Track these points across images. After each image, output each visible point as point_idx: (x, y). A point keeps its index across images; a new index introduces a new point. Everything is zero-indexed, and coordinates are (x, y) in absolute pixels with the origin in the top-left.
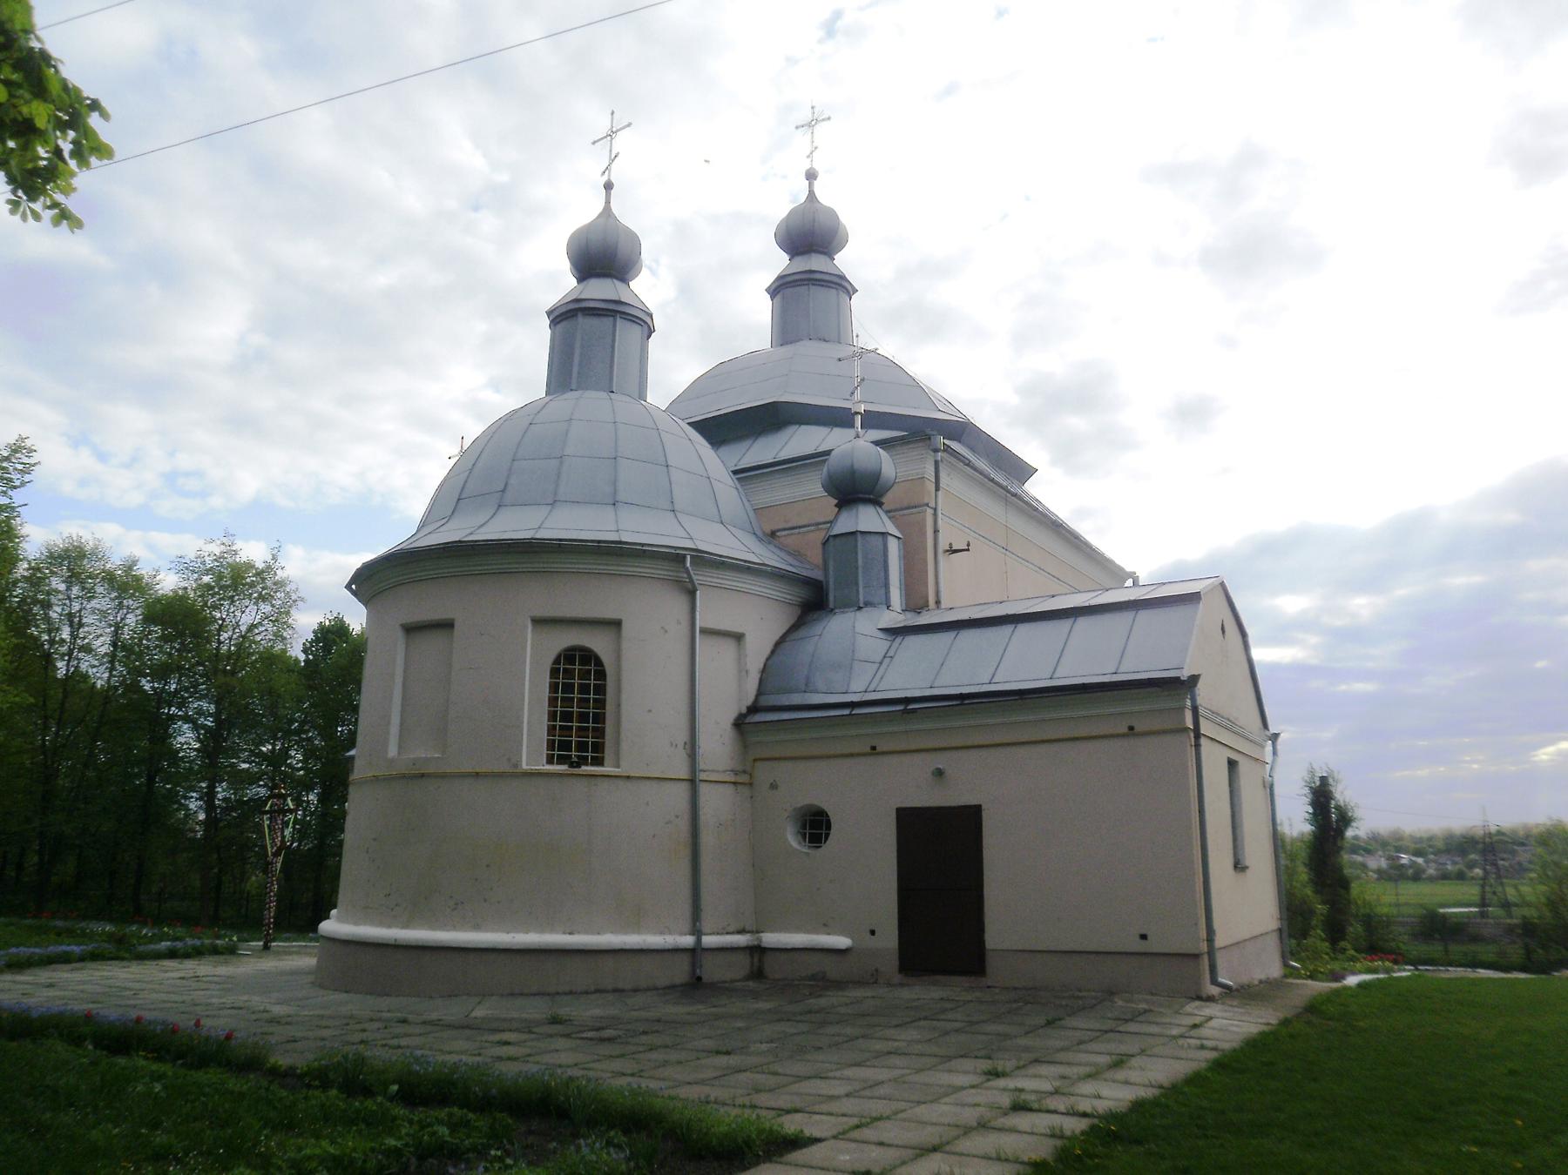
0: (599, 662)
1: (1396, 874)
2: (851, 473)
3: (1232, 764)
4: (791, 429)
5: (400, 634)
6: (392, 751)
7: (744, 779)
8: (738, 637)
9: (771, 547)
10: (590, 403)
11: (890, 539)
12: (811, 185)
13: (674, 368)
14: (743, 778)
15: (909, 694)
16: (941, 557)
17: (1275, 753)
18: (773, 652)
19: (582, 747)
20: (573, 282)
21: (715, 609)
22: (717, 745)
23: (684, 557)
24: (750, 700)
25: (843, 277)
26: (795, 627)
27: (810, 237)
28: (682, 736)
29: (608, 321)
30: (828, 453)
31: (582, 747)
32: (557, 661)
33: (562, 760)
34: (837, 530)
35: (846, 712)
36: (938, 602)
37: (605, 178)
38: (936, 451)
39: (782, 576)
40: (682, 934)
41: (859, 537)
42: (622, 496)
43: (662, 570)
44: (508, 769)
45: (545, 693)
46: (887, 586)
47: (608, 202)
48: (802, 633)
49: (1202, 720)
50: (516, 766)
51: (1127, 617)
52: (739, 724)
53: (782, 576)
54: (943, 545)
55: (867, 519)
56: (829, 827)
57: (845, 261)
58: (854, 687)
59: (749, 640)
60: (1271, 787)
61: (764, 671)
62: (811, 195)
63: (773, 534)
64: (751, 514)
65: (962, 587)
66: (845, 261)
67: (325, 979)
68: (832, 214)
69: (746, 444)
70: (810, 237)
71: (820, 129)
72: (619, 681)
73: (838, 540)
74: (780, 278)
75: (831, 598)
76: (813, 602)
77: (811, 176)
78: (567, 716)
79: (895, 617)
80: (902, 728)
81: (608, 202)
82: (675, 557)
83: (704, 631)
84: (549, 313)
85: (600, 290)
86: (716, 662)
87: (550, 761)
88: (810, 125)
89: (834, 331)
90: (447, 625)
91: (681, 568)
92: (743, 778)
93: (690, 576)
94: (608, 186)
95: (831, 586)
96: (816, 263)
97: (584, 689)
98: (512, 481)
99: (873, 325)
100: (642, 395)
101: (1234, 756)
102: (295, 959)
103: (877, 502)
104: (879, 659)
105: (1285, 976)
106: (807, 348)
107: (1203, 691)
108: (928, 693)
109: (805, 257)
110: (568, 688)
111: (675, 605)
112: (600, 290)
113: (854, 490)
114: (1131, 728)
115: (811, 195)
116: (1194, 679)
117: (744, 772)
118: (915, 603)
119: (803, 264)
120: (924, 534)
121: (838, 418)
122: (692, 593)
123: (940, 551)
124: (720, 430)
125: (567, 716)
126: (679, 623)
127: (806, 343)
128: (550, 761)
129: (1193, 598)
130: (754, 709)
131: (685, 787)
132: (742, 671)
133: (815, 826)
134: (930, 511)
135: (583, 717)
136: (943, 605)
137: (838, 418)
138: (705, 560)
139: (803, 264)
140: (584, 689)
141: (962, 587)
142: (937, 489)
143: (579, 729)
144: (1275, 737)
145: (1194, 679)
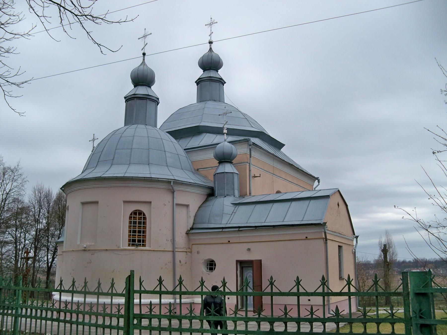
0: (144, 215)
2: (225, 150)
3: (340, 247)
4: (204, 134)
5: (80, 206)
6: (78, 243)
7: (189, 251)
8: (187, 206)
9: (197, 176)
10: (140, 130)
14: (188, 250)
15: (240, 225)
17: (357, 242)
18: (198, 210)
19: (139, 241)
20: (132, 86)
21: (180, 198)
22: (181, 240)
23: (171, 182)
24: (190, 226)
25: (221, 79)
27: (210, 64)
28: (170, 238)
29: (145, 101)
31: (139, 241)
32: (131, 214)
33: (133, 245)
34: (219, 171)
35: (221, 230)
36: (250, 193)
37: (143, 52)
39: (201, 186)
40: (170, 299)
42: (151, 162)
43: (165, 186)
44: (116, 248)
45: (127, 224)
46: (233, 189)
47: (144, 60)
48: (207, 204)
49: (327, 234)
50: (119, 247)
51: (307, 202)
52: (187, 233)
53: (201, 186)
54: (252, 175)
55: (228, 168)
56: (215, 265)
57: (222, 73)
58: (223, 223)
59: (191, 208)
60: (355, 252)
61: (195, 216)
63: (198, 170)
64: (190, 163)
65: (259, 189)
66: (222, 73)
69: (189, 139)
70: (210, 64)
71: (214, 26)
72: (150, 221)
73: (218, 175)
76: (211, 194)
80: (238, 235)
81: (144, 60)
82: (168, 182)
83: (177, 204)
85: (142, 91)
86: (181, 213)
87: (129, 245)
88: (211, 24)
89: (219, 98)
90: (97, 203)
91: (171, 185)
92: (188, 250)
93: (173, 188)
94: (144, 54)
95: (216, 188)
96: (212, 74)
97: (140, 223)
98: (116, 156)
101: (341, 245)
103: (231, 162)
104: (231, 213)
105: (436, 325)
106: (210, 104)
107: (329, 226)
109: (208, 71)
110: (135, 223)
111: (167, 197)
112: (142, 91)
113: (224, 158)
116: (325, 224)
117: (189, 248)
118: (242, 195)
120: (246, 170)
121: (218, 131)
122: (173, 192)
124: (177, 134)
125: (130, 235)
126: (169, 202)
127: (209, 102)
128: (129, 245)
129: (327, 197)
130: (192, 229)
131: (171, 253)
132: (188, 217)
133: (211, 265)
134: (248, 164)
135: (139, 232)
136: (252, 194)
137: (218, 131)
138: (177, 182)
140: (140, 223)
141: (259, 189)
142: (250, 157)
143: (138, 235)
144: (357, 237)
145: (325, 224)
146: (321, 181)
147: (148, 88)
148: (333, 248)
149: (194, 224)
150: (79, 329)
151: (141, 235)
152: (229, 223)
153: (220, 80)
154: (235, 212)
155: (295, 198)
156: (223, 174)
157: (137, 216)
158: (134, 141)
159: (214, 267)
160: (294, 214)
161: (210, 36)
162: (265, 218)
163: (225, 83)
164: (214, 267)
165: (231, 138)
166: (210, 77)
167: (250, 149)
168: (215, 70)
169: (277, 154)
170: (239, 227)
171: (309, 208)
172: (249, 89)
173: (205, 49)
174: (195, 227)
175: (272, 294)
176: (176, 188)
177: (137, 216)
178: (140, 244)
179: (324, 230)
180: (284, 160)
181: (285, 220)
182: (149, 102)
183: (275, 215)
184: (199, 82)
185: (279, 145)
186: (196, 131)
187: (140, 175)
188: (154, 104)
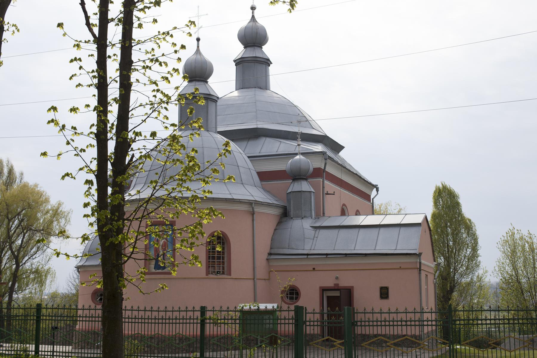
1: (447, 343)
12: (253, 13)
16: (325, 195)
36: (324, 213)
39: (277, 207)
46: (311, 210)
47: (198, 47)
66: (268, 50)
73: (294, 193)
75: (292, 214)
81: (198, 47)
82: (250, 203)
99: (282, 81)
108: (333, 252)
109: (252, 49)
114: (314, 269)
131: (252, 281)
136: (326, 215)
138: (257, 203)
146: (380, 189)
149: (271, 248)
150: (507, 355)
158: (205, 153)
162: (354, 245)
163: (271, 63)
169: (335, 158)
170: (327, 254)
175: (125, 310)
176: (257, 209)
179: (420, 260)
181: (377, 248)
185: (337, 148)
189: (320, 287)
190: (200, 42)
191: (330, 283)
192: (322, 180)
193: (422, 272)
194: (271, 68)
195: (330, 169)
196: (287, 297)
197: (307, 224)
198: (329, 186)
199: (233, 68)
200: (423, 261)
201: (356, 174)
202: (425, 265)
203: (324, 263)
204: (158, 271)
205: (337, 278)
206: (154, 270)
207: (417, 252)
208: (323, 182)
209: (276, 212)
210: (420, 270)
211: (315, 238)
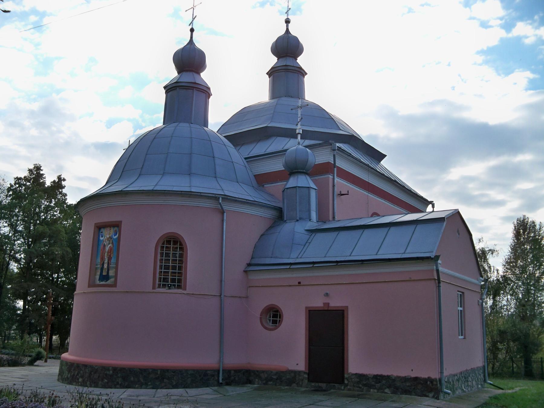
4: (274, 138)
11: (311, 189)
12: (287, 26)
13: (219, 114)
19: (173, 280)
23: (219, 198)
25: (301, 68)
26: (271, 227)
27: (287, 49)
30: (286, 150)
33: (164, 286)
36: (334, 218)
37: (191, 27)
38: (334, 150)
39: (270, 207)
41: (298, 188)
46: (309, 211)
47: (192, 37)
53: (270, 207)
54: (337, 191)
57: (301, 61)
62: (287, 31)
65: (344, 213)
66: (301, 61)
67: (62, 377)
68: (296, 39)
69: (253, 145)
70: (287, 49)
73: (289, 190)
74: (272, 68)
75: (285, 216)
77: (287, 22)
78: (167, 267)
79: (313, 224)
81: (192, 37)
82: (215, 198)
84: (165, 88)
85: (188, 78)
89: (297, 91)
94: (192, 30)
96: (289, 62)
99: (315, 91)
100: (206, 124)
102: (50, 369)
108: (323, 260)
112: (188, 78)
114: (299, 283)
115: (287, 31)
118: (322, 218)
119: (284, 62)
122: (223, 212)
123: (336, 194)
124: (237, 140)
130: (249, 265)
135: (174, 268)
138: (227, 198)
139: (284, 62)
141: (344, 213)
143: (172, 273)
147: (196, 75)
148: (449, 295)
149: (252, 258)
151: (175, 273)
152: (299, 257)
153: (299, 70)
154: (309, 241)
155: (395, 221)
156: (295, 189)
157: (172, 246)
159: (278, 319)
160: (392, 246)
161: (286, 13)
162: (351, 251)
163: (306, 74)
164: (278, 319)
165: (308, 142)
166: (286, 66)
167: (334, 156)
168: (292, 57)
170: (314, 263)
171: (414, 236)
172: (344, 91)
173: (282, 32)
174: (253, 262)
176: (227, 207)
177: (172, 246)
178: (174, 285)
179: (437, 267)
180: (383, 175)
182: (195, 92)
183: (365, 247)
184: (272, 73)
185: (379, 156)
186: (265, 134)
187: (175, 189)
188: (203, 95)
189: (306, 308)
190: (194, 33)
191: (318, 303)
192: (331, 177)
193: (441, 284)
194: (306, 77)
195: (341, 163)
196: (270, 320)
197: (300, 228)
198: (341, 184)
199: (266, 80)
200: (440, 269)
201: (395, 181)
202: (444, 273)
203: (311, 275)
204: (102, 283)
205: (327, 295)
206: (98, 282)
207: (432, 255)
208: (334, 179)
209: (269, 214)
210: (439, 283)
211: (307, 244)
